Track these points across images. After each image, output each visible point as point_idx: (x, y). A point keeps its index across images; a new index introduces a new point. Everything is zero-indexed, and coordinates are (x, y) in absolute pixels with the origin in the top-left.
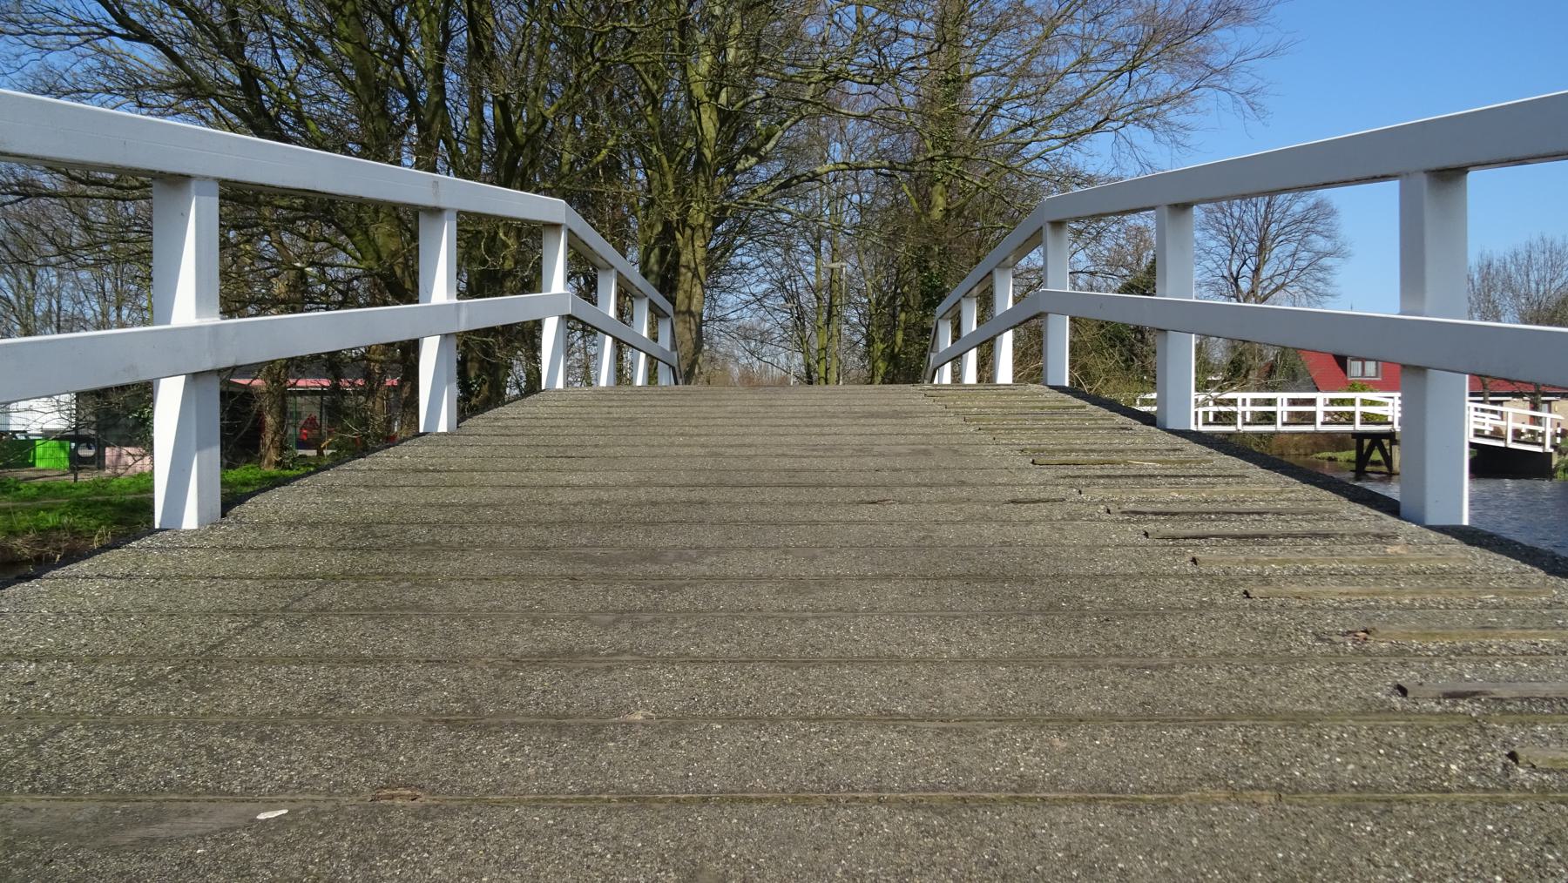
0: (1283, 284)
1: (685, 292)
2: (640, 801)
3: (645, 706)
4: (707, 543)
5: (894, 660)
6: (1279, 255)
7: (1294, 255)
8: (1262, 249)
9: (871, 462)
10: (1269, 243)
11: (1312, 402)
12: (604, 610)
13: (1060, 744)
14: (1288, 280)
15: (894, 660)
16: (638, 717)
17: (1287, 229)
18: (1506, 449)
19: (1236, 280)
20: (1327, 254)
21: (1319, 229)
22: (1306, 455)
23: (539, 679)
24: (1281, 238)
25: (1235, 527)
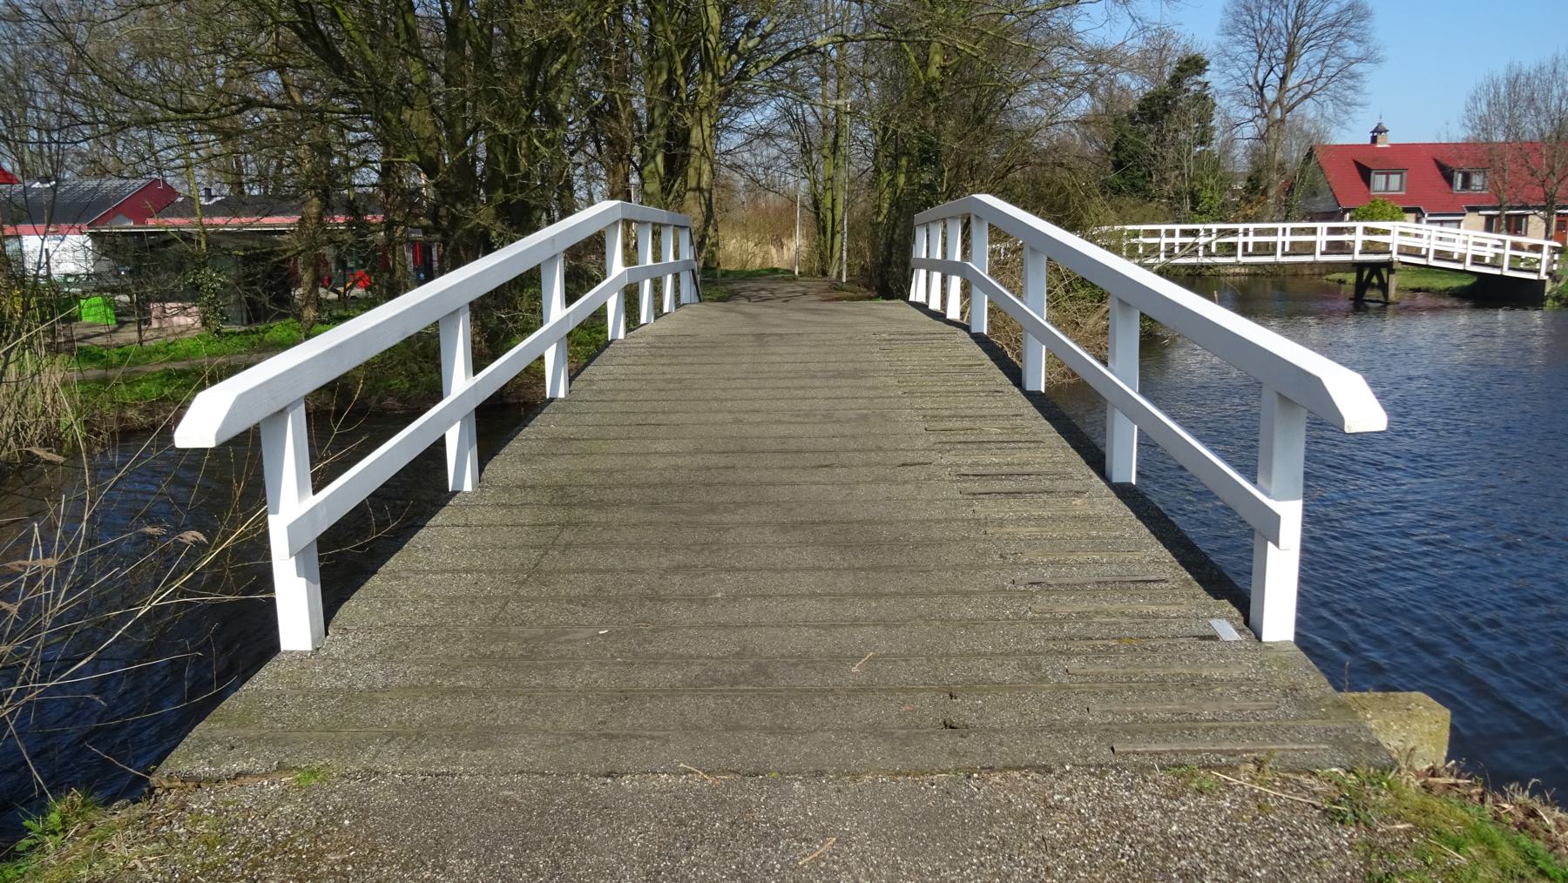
0: (1311, 93)
1: (696, 169)
2: (725, 626)
3: (721, 591)
4: (738, 499)
5: (820, 569)
6: (1308, 60)
7: (1324, 60)
8: (1290, 56)
9: (832, 429)
10: (1297, 48)
11: (1314, 231)
12: (695, 544)
13: (874, 604)
14: (1315, 89)
15: (820, 569)
16: (719, 595)
17: (1319, 33)
18: (1501, 276)
19: (1261, 89)
20: (1359, 60)
21: (1352, 34)
22: (1320, 275)
23: (677, 579)
24: (1312, 42)
25: (1009, 485)
